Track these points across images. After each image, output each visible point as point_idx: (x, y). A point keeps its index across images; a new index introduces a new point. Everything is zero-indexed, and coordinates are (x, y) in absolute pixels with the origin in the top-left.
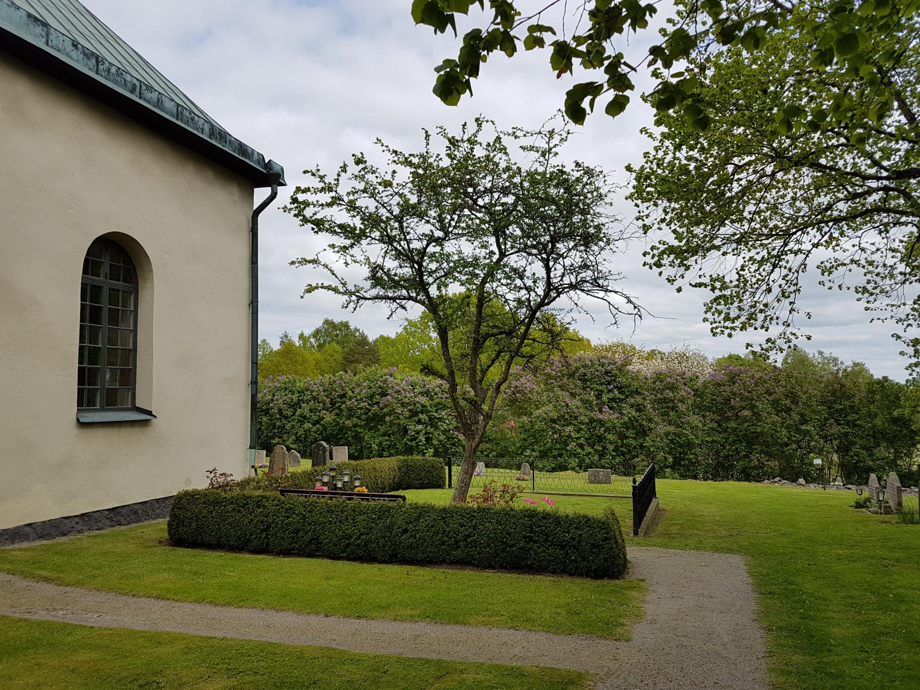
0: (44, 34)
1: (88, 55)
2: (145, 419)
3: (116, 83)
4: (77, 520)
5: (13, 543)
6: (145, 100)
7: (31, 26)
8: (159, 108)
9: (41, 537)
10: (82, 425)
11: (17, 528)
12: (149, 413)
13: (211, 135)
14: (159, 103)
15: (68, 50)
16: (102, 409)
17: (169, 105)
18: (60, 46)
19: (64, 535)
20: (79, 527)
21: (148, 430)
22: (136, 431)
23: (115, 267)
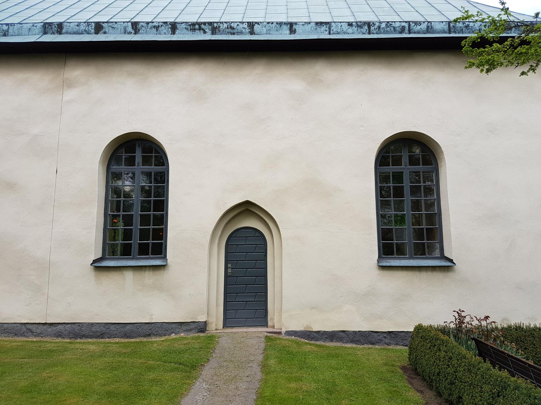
0: (327, 29)
1: (360, 25)
2: (447, 266)
3: (387, 32)
4: (385, 335)
5: (332, 341)
6: (415, 33)
7: (318, 29)
8: (430, 33)
9: (352, 342)
10: (383, 268)
11: (333, 332)
12: (451, 261)
13: (292, 31)
14: (429, 29)
15: (345, 30)
16: (411, 258)
17: (438, 27)
18: (339, 31)
19: (373, 344)
20: (387, 341)
21: (450, 274)
22: (438, 276)
23: (137, 158)
